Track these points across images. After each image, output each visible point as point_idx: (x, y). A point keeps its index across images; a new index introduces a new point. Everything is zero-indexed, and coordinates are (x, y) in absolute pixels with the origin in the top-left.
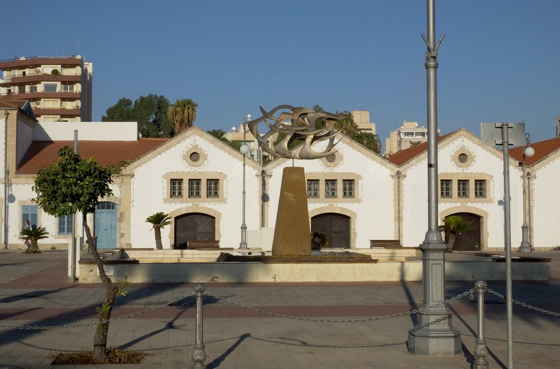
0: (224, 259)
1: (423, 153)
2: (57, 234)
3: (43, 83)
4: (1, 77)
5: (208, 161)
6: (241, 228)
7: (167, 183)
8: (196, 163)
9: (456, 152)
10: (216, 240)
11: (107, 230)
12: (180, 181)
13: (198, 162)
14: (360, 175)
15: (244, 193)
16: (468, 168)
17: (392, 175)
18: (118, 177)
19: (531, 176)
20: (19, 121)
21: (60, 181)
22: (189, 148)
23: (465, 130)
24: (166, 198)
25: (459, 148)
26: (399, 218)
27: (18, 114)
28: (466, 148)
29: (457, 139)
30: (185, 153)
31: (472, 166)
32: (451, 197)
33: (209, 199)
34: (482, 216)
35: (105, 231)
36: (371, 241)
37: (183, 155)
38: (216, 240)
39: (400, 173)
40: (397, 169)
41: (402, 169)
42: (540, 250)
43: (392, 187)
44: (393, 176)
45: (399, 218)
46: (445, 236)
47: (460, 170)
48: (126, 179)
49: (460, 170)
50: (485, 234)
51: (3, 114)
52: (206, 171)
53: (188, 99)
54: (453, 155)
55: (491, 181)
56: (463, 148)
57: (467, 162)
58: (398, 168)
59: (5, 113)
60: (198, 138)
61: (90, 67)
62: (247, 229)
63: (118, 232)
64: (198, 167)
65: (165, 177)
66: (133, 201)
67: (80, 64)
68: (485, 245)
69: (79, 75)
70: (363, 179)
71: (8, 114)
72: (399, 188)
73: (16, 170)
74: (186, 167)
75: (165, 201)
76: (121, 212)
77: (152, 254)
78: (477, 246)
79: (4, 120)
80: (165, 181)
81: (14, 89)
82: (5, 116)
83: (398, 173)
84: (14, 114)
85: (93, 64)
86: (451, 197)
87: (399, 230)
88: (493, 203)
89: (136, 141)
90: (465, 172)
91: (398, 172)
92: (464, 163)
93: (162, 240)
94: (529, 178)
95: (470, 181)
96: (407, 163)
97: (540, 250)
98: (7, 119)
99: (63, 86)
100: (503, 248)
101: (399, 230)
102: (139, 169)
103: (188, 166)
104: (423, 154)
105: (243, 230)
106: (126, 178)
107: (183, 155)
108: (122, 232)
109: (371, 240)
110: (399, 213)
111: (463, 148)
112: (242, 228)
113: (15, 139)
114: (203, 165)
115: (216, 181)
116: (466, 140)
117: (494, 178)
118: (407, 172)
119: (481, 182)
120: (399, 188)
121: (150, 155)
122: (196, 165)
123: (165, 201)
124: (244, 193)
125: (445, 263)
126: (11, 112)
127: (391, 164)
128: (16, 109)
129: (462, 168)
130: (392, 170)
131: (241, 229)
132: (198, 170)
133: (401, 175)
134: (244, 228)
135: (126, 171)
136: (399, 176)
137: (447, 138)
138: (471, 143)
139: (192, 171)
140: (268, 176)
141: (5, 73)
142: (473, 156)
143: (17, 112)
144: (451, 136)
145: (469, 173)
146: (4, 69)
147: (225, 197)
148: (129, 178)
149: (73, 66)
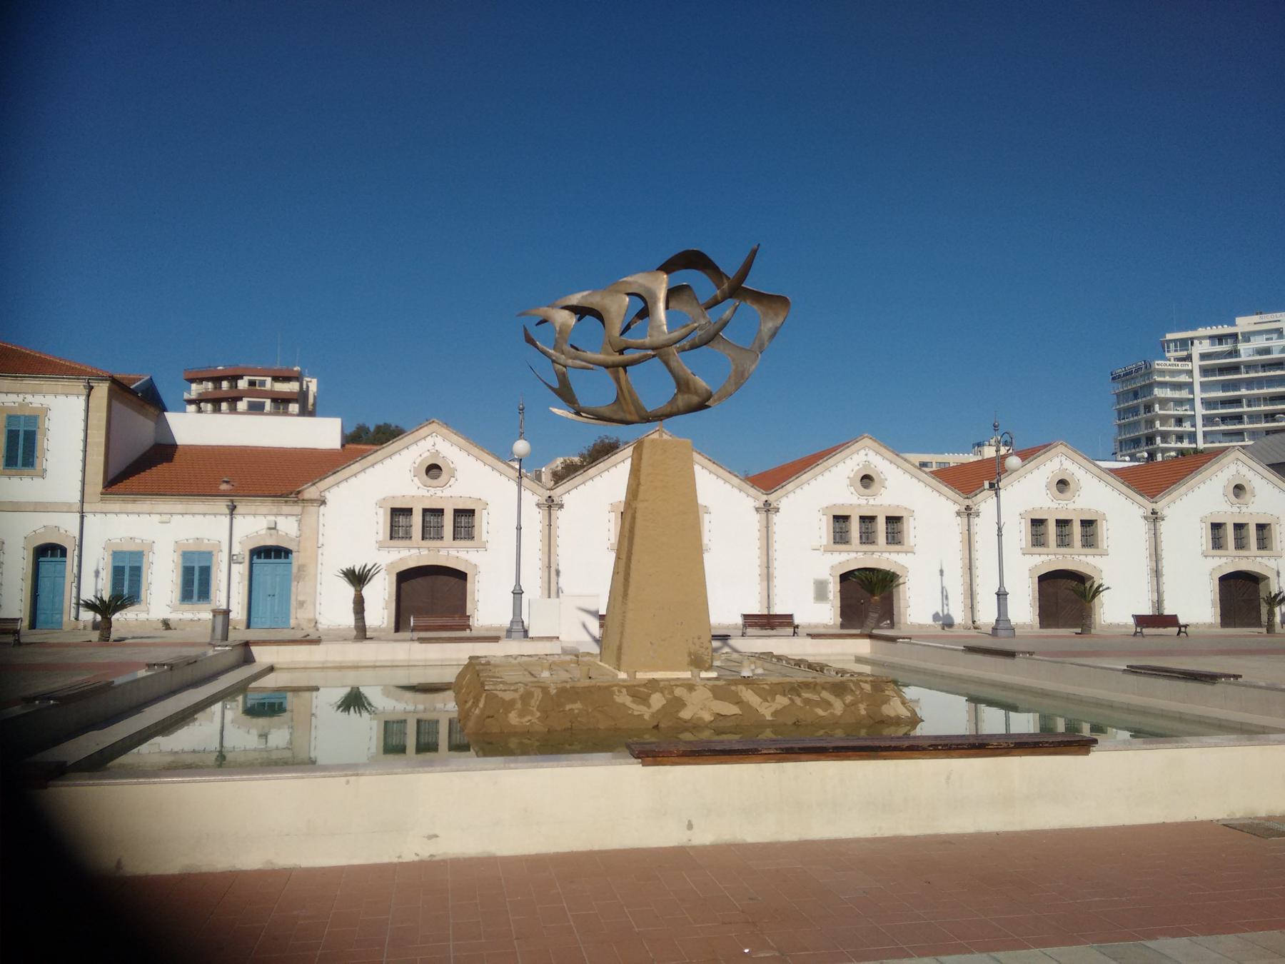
2: (178, 602)
3: (245, 400)
4: (189, 390)
5: (456, 480)
6: (512, 592)
7: (385, 514)
8: (436, 481)
9: (856, 472)
10: (468, 614)
11: (274, 595)
12: (408, 512)
13: (440, 479)
14: (705, 506)
15: (519, 528)
17: (757, 506)
18: (296, 504)
19: (973, 511)
20: (116, 404)
22: (423, 456)
24: (381, 539)
25: (861, 466)
26: (768, 577)
27: (110, 391)
28: (873, 466)
29: (857, 452)
30: (416, 466)
33: (458, 543)
35: (269, 599)
37: (414, 467)
38: (468, 614)
39: (770, 505)
40: (765, 498)
41: (772, 498)
43: (757, 526)
44: (759, 508)
45: (768, 577)
46: (841, 605)
47: (863, 501)
48: (312, 509)
49: (863, 501)
50: (902, 602)
51: (82, 387)
52: (452, 495)
54: (851, 476)
55: (911, 519)
56: (867, 464)
58: (765, 496)
59: (84, 386)
60: (439, 440)
61: (313, 386)
62: (523, 595)
63: (293, 597)
64: (438, 488)
65: (380, 504)
66: (323, 545)
67: (298, 378)
68: (902, 621)
69: (295, 391)
71: (91, 388)
72: (767, 527)
73: (104, 487)
74: (418, 488)
75: (381, 546)
76: (300, 563)
77: (809, 635)
79: (82, 399)
80: (381, 511)
81: (206, 407)
82: (85, 392)
84: (102, 390)
85: (318, 381)
87: (769, 596)
88: (914, 553)
89: (338, 450)
90: (870, 503)
91: (766, 501)
93: (366, 614)
94: (969, 515)
98: (88, 396)
99: (273, 404)
101: (769, 596)
102: (335, 490)
103: (421, 486)
105: (516, 595)
106: (310, 504)
107: (414, 467)
108: (301, 598)
109: (744, 615)
110: (768, 567)
111: (867, 464)
112: (515, 592)
113: (103, 432)
114: (448, 485)
115: (470, 513)
116: (871, 453)
117: (916, 514)
120: (767, 527)
121: (355, 467)
122: (435, 485)
123: (381, 546)
124: (519, 528)
125: (80, 609)
126: (96, 384)
127: (756, 489)
128: (106, 380)
129: (866, 498)
130: (756, 499)
131: (512, 594)
132: (439, 494)
133: (772, 507)
134: (518, 593)
135: (311, 492)
136: (768, 509)
138: (879, 458)
139: (429, 494)
140: (557, 504)
141: (194, 386)
142: (882, 479)
143: (108, 385)
145: (876, 506)
146: (192, 381)
147: (484, 539)
148: (315, 505)
149: (287, 379)
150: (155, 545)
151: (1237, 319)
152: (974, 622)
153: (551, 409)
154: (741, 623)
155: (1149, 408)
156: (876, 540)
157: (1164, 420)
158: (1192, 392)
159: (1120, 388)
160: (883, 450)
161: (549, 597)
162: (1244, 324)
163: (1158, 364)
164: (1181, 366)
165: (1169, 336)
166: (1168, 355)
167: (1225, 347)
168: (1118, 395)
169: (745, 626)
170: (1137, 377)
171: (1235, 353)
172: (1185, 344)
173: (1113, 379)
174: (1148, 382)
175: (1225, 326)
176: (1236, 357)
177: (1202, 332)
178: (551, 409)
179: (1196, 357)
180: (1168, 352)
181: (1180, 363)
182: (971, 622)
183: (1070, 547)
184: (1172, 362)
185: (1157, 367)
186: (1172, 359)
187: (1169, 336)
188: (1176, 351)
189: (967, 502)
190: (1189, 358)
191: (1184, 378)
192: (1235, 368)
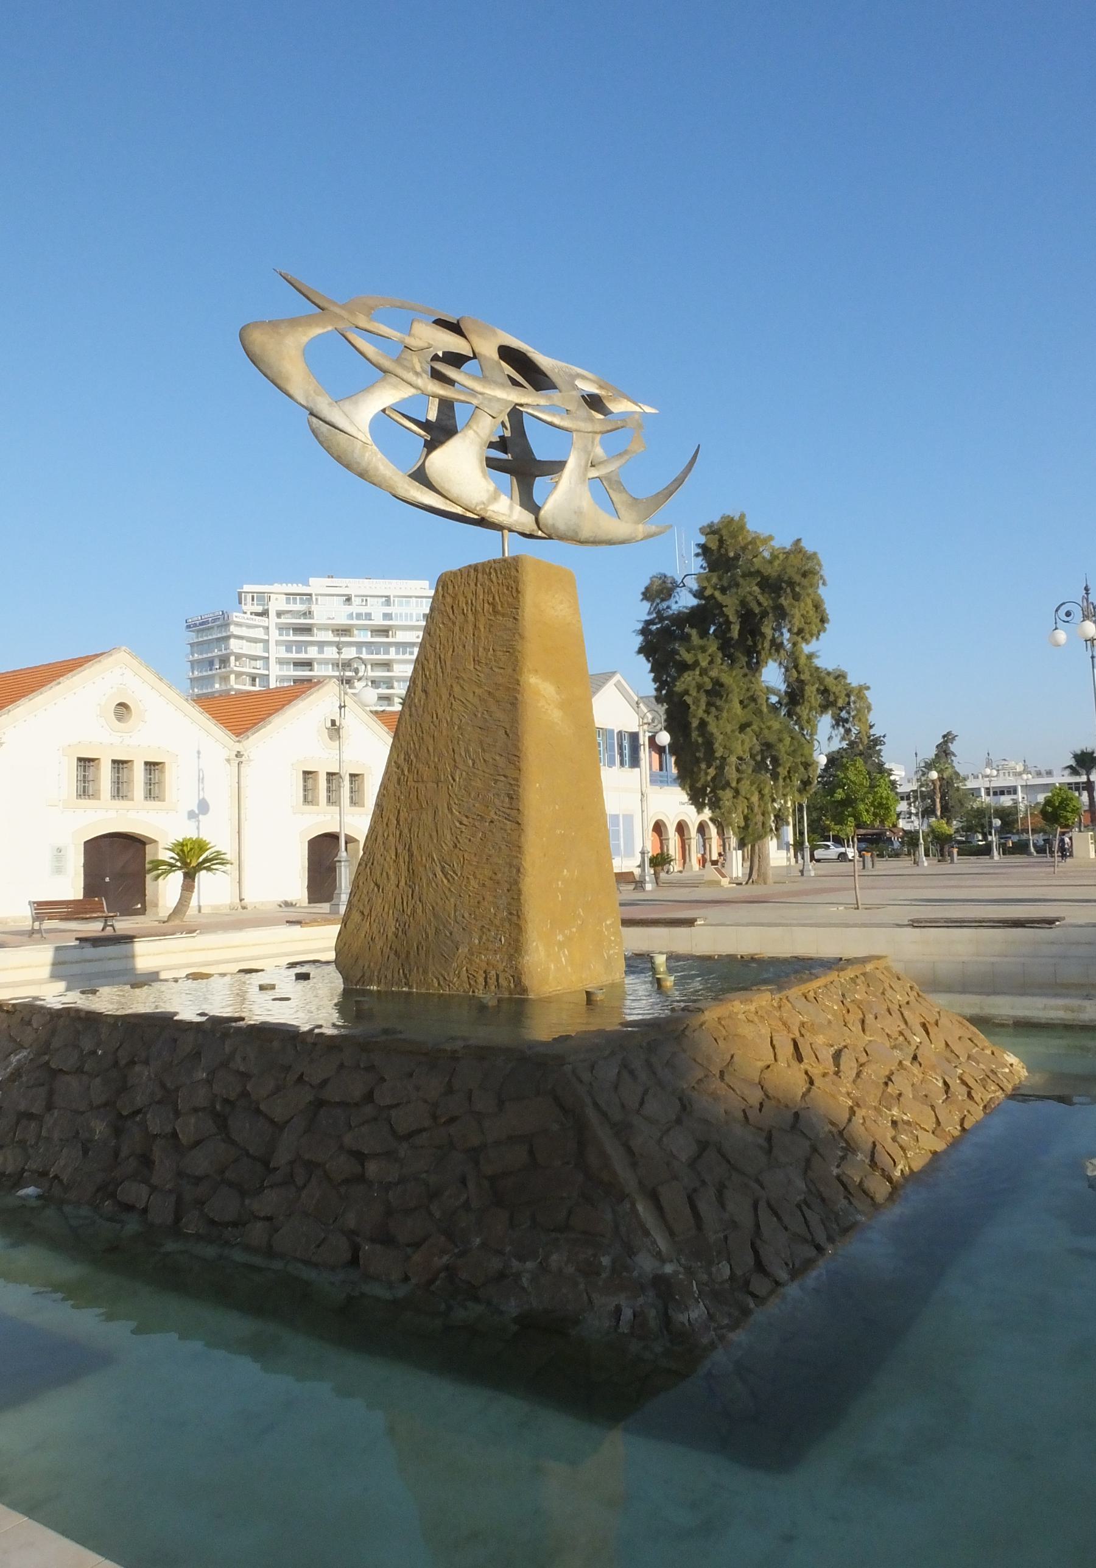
0: (1035, 841)
1: (41, 694)
16: (131, 734)
21: (780, 792)
23: (128, 650)
31: (139, 731)
32: (95, 796)
34: (357, 838)
36: (778, 849)
42: (255, 907)
53: (818, 731)
57: (131, 722)
70: (228, 760)
78: (139, 906)
83: (239, 755)
86: (95, 796)
92: (123, 723)
95: (102, 761)
96: (4, 714)
97: (255, 907)
100: (26, 917)
104: (42, 695)
118: (4, 733)
119: (120, 765)
129: (120, 734)
137: (93, 664)
144: (100, 661)
150: (803, 544)
151: (311, 579)
152: (241, 900)
153: (657, 412)
154: (30, 914)
155: (224, 661)
156: (129, 794)
157: (239, 675)
158: (267, 650)
159: (193, 637)
160: (143, 670)
161: (621, 905)
162: (317, 585)
163: (236, 617)
164: (259, 621)
165: (247, 588)
166: (244, 608)
167: (299, 607)
168: (192, 645)
169: (38, 918)
170: (212, 628)
171: (308, 614)
172: (261, 597)
173: (188, 627)
174: (224, 634)
175: (300, 585)
176: (310, 618)
177: (277, 587)
178: (657, 412)
179: (272, 614)
180: (245, 604)
181: (257, 618)
182: (238, 901)
183: (359, 806)
184: (248, 615)
185: (235, 619)
186: (249, 613)
187: (247, 588)
188: (253, 604)
189: (238, 747)
190: (265, 613)
191: (259, 634)
192: (307, 630)
